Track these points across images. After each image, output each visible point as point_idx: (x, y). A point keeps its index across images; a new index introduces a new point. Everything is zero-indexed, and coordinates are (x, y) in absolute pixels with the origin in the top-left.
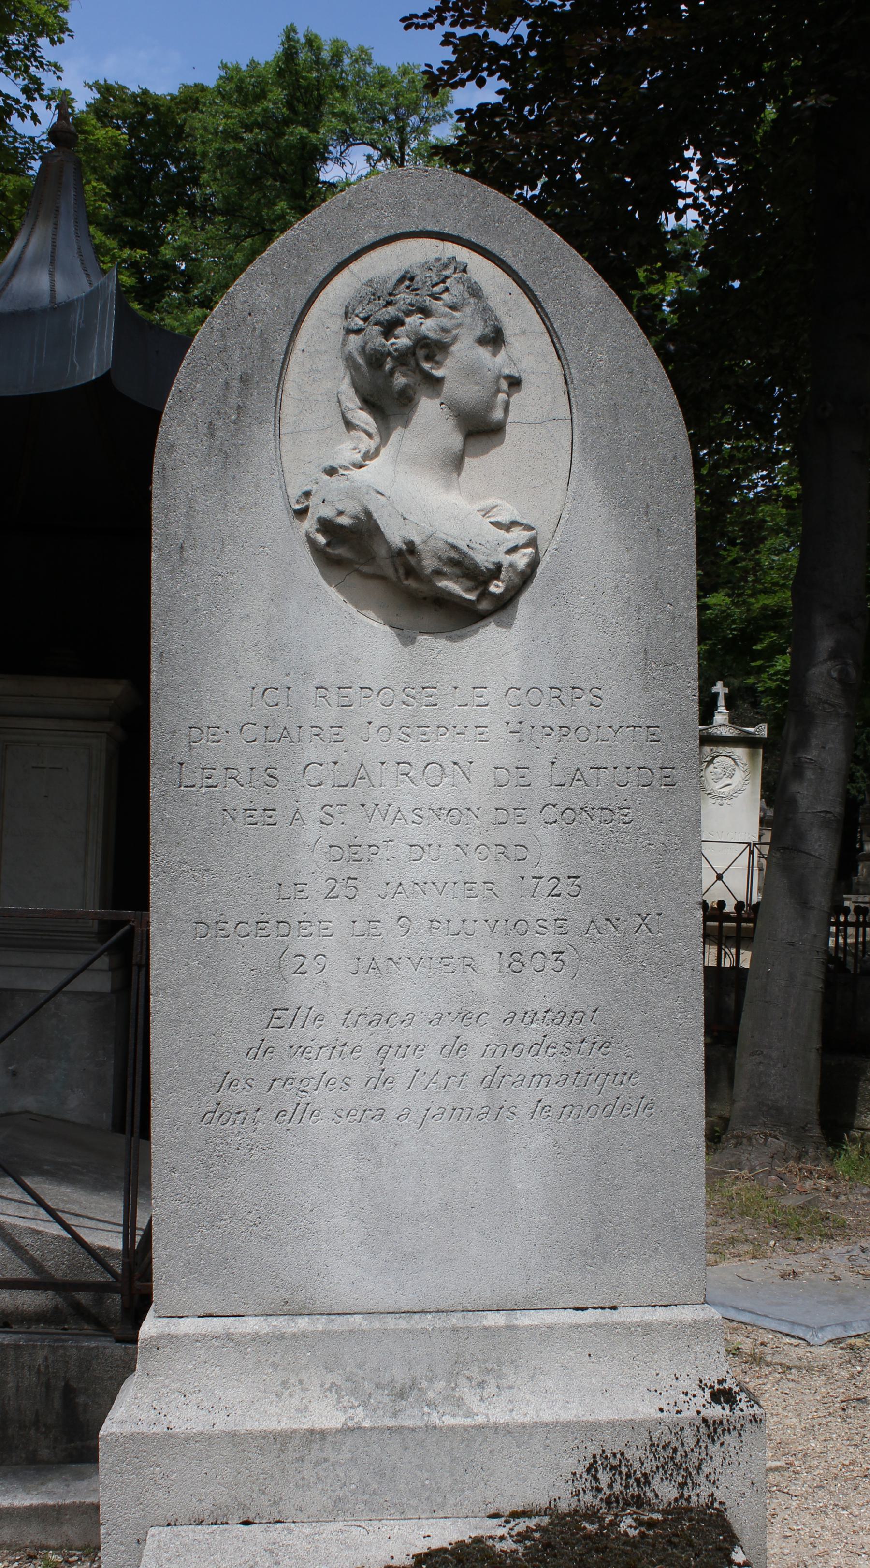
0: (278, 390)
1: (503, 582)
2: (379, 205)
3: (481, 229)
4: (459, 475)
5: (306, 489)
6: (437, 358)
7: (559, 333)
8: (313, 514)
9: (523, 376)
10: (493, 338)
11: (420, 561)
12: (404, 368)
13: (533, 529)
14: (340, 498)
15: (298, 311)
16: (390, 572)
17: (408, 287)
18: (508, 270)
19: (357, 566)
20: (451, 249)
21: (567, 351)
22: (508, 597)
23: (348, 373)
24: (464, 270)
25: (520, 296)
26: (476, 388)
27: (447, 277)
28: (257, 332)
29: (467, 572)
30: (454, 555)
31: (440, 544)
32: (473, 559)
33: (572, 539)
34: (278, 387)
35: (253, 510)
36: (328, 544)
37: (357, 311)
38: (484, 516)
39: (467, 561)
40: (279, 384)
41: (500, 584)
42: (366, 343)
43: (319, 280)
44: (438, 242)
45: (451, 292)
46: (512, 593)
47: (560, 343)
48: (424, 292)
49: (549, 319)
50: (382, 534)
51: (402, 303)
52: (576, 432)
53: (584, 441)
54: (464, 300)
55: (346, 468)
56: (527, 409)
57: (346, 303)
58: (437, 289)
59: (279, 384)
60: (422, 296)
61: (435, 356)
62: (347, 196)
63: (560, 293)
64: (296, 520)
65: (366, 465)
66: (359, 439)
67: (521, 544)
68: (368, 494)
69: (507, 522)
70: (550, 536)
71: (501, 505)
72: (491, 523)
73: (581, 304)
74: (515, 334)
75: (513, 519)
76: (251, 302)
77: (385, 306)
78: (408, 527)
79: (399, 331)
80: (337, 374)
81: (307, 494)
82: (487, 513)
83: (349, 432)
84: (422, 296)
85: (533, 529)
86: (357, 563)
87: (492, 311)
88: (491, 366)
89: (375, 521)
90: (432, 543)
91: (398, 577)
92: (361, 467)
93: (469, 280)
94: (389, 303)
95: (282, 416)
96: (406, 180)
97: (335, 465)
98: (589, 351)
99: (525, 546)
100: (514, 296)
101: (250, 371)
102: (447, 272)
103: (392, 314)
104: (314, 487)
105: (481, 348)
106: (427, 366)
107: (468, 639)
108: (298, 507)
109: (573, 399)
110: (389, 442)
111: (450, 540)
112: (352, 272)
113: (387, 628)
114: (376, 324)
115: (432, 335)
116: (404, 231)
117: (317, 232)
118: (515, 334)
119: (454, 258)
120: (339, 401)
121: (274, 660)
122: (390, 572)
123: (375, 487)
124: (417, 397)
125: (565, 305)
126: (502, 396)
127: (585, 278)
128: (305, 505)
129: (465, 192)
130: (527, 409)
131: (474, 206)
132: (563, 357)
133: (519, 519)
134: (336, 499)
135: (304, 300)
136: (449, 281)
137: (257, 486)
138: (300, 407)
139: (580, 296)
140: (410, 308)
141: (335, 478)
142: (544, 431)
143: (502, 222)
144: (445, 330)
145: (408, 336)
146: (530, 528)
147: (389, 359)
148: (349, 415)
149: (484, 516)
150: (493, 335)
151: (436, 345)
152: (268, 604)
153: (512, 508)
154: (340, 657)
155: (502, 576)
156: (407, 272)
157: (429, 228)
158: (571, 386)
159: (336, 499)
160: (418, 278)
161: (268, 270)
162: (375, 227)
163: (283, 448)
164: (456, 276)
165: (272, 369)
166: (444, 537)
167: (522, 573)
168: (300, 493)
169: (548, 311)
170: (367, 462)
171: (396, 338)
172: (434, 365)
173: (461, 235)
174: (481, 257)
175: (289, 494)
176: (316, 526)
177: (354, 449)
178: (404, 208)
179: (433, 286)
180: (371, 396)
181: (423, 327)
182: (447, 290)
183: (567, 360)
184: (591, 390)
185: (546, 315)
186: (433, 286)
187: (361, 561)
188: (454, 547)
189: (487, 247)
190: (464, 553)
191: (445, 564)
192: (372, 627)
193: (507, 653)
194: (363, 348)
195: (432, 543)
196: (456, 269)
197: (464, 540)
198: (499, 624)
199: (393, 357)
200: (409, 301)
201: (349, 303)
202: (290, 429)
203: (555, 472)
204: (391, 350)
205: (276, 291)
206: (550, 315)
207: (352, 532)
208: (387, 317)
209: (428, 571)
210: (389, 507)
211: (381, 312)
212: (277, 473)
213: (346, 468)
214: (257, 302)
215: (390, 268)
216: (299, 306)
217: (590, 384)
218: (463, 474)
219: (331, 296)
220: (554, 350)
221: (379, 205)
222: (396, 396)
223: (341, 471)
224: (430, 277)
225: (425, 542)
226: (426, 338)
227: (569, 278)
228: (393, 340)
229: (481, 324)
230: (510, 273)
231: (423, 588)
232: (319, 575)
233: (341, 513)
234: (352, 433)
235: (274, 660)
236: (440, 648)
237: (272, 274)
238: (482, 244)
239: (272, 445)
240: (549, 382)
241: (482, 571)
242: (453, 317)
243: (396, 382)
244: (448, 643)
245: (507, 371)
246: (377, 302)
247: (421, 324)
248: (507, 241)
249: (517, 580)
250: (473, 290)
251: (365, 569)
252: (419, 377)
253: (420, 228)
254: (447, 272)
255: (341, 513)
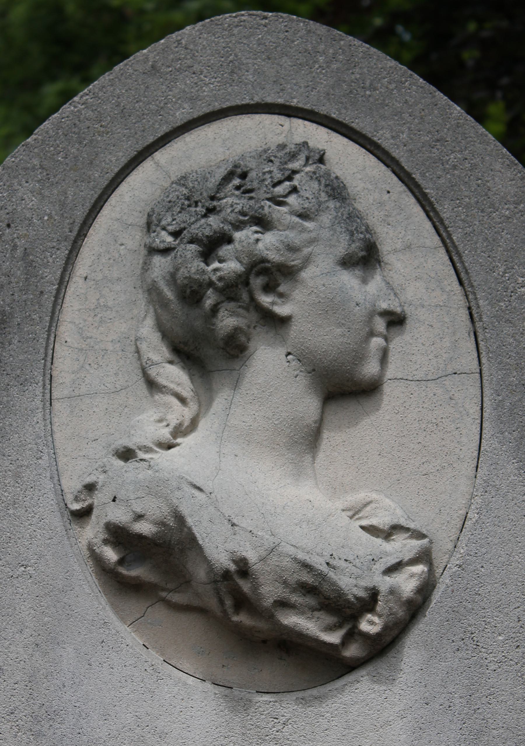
0: (49, 335)
1: (380, 616)
2: (197, 67)
3: (344, 100)
4: (314, 458)
5: (89, 480)
6: (281, 289)
7: (461, 248)
8: (98, 517)
9: (408, 310)
10: (363, 258)
11: (255, 588)
12: (232, 305)
13: (424, 536)
14: (139, 494)
15: (79, 221)
16: (212, 603)
17: (238, 188)
18: (384, 158)
19: (164, 594)
20: (301, 129)
21: (473, 274)
22: (389, 639)
23: (152, 310)
24: (321, 160)
25: (404, 196)
26: (339, 331)
27: (295, 172)
28: (19, 252)
29: (327, 602)
30: (307, 578)
31: (286, 563)
32: (334, 584)
33: (484, 550)
34: (49, 331)
35: (11, 512)
36: (121, 562)
37: (164, 223)
38: (351, 517)
39: (325, 587)
40: (50, 326)
41: (376, 619)
42: (177, 269)
43: (110, 176)
44: (282, 119)
45: (302, 193)
46: (396, 632)
47: (462, 262)
48: (261, 194)
49: (446, 228)
50: (200, 549)
51: (229, 210)
52: (487, 392)
53: (499, 405)
54: (320, 204)
55: (147, 450)
56: (414, 358)
57: (148, 209)
58: (279, 190)
59: (50, 326)
60: (258, 201)
61: (278, 285)
62: (151, 55)
63: (460, 190)
64: (74, 526)
65: (178, 445)
66: (168, 406)
67: (406, 559)
68: (179, 489)
69: (386, 527)
70: (450, 546)
71: (377, 501)
72: (362, 527)
73: (492, 205)
74: (395, 251)
75: (395, 521)
76: (10, 209)
77: (205, 216)
78: (237, 537)
79: (225, 250)
80: (135, 312)
81: (90, 488)
82: (359, 511)
83: (152, 395)
84: (258, 201)
85: (424, 536)
86: (163, 590)
87: (361, 218)
88: (360, 298)
89: (190, 529)
90: (274, 560)
91: (225, 612)
92: (170, 447)
93: (328, 174)
94: (210, 211)
95: (54, 373)
96: (236, 31)
97: (131, 445)
98: (505, 273)
99: (413, 562)
100: (394, 196)
101: (7, 308)
102: (295, 165)
103: (215, 226)
104: (102, 478)
105: (345, 272)
106: (266, 300)
107: (329, 702)
108: (76, 506)
109: (482, 344)
110: (212, 411)
111: (301, 556)
112: (157, 164)
113: (208, 685)
114: (191, 242)
115: (274, 257)
116: (233, 104)
117: (107, 107)
118: (395, 251)
119: (305, 144)
120: (138, 351)
121: (38, 735)
122: (212, 603)
123: (190, 479)
124: (252, 345)
125: (468, 206)
126: (377, 342)
127: (498, 166)
128: (86, 504)
129: (322, 47)
130: (414, 358)
131: (334, 66)
132: (466, 283)
133: (403, 522)
134: (132, 497)
135: (88, 205)
136: (297, 177)
137: (17, 476)
138: (82, 359)
139: (490, 193)
140: (241, 218)
141: (131, 465)
142: (439, 391)
143: (375, 89)
144: (292, 249)
145: (238, 259)
146: (420, 536)
147: (210, 292)
148: (152, 372)
149: (351, 517)
150: (363, 253)
151: (279, 270)
152: (30, 651)
153: (393, 505)
154: (138, 731)
155: (378, 609)
156: (236, 166)
157: (269, 100)
158: (478, 325)
159: (132, 497)
160: (252, 175)
161: (36, 162)
162: (192, 100)
163: (55, 420)
164: (308, 169)
165: (41, 306)
166: (292, 551)
167: (409, 602)
168: (79, 487)
169: (444, 216)
170: (179, 440)
171: (220, 261)
172: (277, 299)
173: (316, 109)
174: (345, 140)
175: (65, 487)
176: (102, 536)
177: (160, 421)
178: (232, 72)
179: (275, 185)
180: (186, 344)
181: (260, 245)
182: (294, 190)
183: (472, 286)
184: (508, 329)
185: (442, 221)
186: (275, 185)
187: (169, 586)
188: (306, 566)
189: (354, 125)
190: (322, 576)
191: (294, 591)
192: (185, 684)
193: (388, 723)
194: (173, 276)
195: (274, 560)
196: (308, 159)
197: (322, 556)
198: (376, 679)
199: (216, 289)
200: (239, 208)
201: (153, 210)
202: (66, 392)
203: (457, 451)
204: (214, 278)
205: (47, 193)
206: (446, 222)
207: (156, 545)
208: (208, 232)
209: (268, 602)
210: (212, 509)
211: (198, 225)
212: (46, 457)
213: (147, 450)
214: (19, 209)
215: (213, 157)
216: (80, 214)
217: (508, 321)
218: (321, 455)
219: (127, 199)
220: (453, 272)
221: (197, 67)
222: (221, 344)
223: (141, 455)
224: (270, 172)
225: (263, 559)
226: (264, 260)
227: (474, 167)
228: (216, 265)
229: (344, 238)
230: (388, 162)
231: (261, 625)
232: (108, 608)
233: (139, 517)
234: (157, 397)
235: (38, 735)
236: (288, 716)
237: (42, 167)
238: (347, 120)
239: (40, 415)
240: (447, 319)
241: (348, 601)
242: (304, 230)
243: (220, 325)
244: (300, 709)
245: (384, 306)
246: (193, 209)
247: (258, 240)
248: (383, 117)
249: (401, 613)
250: (333, 189)
251: (176, 598)
252: (254, 316)
253: (257, 99)
254: (295, 165)
255: (139, 517)
